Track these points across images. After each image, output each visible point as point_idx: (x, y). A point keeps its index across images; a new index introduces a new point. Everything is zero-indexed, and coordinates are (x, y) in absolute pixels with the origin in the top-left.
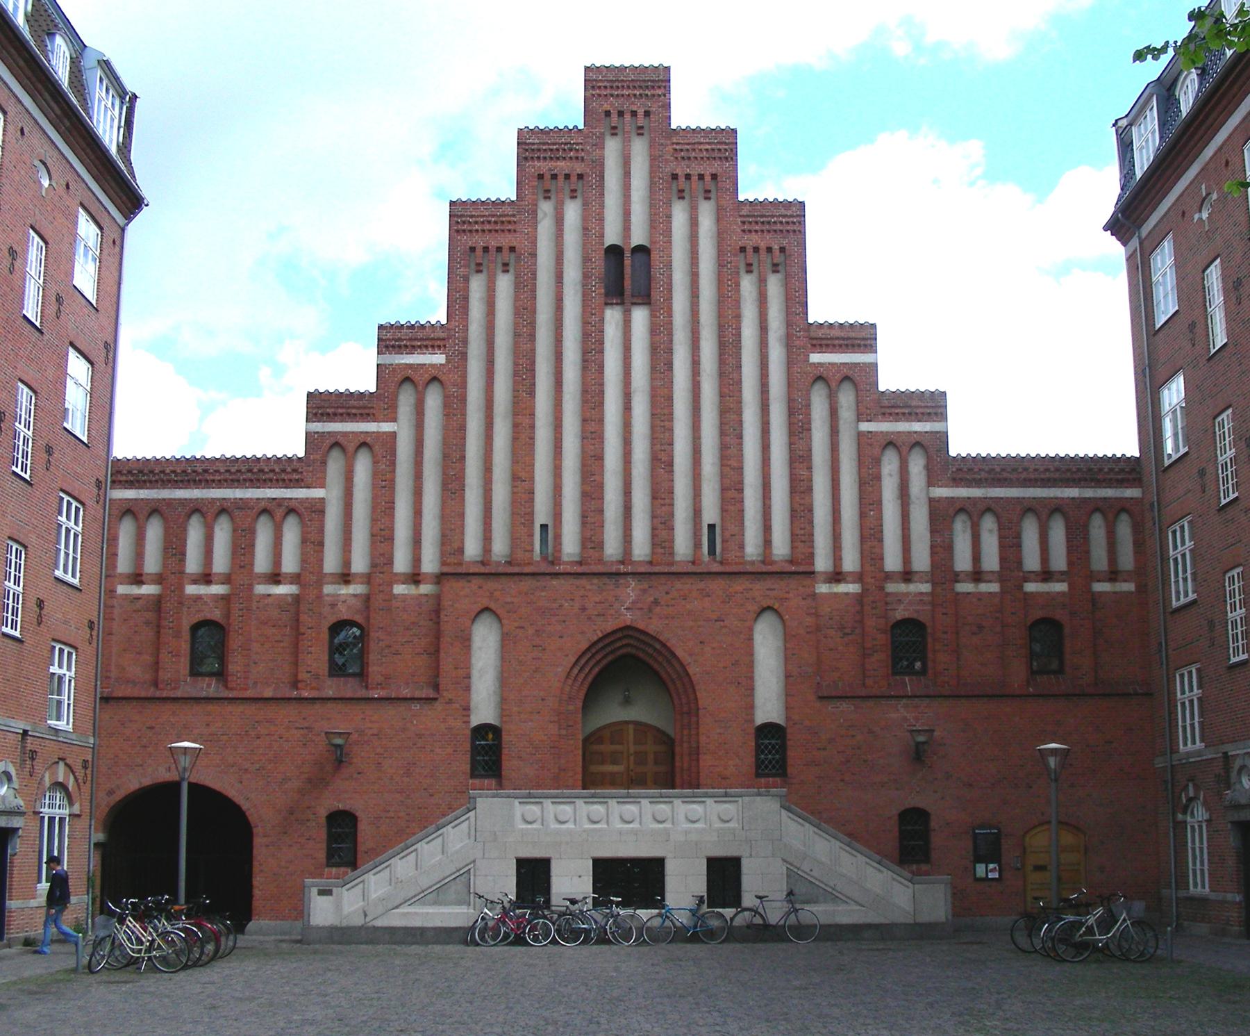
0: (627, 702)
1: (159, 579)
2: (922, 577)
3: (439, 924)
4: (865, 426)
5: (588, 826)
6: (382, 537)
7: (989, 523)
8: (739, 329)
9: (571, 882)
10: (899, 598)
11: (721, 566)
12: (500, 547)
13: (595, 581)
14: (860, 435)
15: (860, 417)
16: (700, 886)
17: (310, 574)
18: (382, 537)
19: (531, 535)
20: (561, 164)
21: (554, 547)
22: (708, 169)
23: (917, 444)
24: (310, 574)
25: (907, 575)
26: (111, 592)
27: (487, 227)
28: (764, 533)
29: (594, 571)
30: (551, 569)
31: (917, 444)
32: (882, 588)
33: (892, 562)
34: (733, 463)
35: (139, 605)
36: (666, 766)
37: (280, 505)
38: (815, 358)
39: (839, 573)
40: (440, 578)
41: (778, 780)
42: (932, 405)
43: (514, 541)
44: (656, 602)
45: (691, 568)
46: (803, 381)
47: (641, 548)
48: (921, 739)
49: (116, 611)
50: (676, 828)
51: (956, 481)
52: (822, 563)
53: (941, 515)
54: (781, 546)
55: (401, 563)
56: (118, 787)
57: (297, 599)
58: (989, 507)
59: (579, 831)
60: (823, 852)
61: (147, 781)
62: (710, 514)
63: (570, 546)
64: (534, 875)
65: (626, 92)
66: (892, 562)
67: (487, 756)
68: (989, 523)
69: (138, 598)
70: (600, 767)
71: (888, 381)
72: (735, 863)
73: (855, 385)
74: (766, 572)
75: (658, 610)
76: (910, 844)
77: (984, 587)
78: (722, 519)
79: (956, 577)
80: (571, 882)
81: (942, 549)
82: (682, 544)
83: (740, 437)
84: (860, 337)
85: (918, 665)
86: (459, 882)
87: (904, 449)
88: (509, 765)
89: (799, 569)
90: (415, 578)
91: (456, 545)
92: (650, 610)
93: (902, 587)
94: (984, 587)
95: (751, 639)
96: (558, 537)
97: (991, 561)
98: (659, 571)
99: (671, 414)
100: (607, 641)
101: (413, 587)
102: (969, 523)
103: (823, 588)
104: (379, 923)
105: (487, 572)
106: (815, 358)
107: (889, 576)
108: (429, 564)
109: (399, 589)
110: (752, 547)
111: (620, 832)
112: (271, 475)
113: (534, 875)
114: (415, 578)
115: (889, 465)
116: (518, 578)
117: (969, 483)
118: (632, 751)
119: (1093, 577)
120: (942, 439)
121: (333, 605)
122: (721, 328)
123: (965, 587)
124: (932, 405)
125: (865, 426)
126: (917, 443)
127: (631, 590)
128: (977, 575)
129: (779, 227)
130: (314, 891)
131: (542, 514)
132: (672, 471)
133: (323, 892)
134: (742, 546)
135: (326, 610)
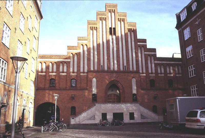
0: (112, 91)
1: (45, 72)
2: (65, 72)
3: (90, 123)
4: (145, 53)
5: (112, 108)
6: (79, 67)
7: (65, 65)
8: (128, 39)
9: (110, 117)
10: (151, 76)
11: (127, 71)
12: (96, 68)
13: (109, 73)
14: (145, 54)
15: (145, 52)
16: (101, 117)
17: (68, 72)
18: (79, 67)
19: (100, 67)
20: (103, 16)
21: (103, 69)
22: (123, 18)
23: (152, 55)
24: (68, 72)
25: (152, 73)
26: (38, 74)
27: (93, 24)
28: (133, 67)
29: (109, 72)
30: (103, 71)
31: (152, 55)
32: (149, 75)
33: (71, 70)
34: (118, 56)
35: (42, 76)
36: (119, 100)
37: (63, 62)
38: (138, 43)
39: (64, 72)
40: (87, 73)
41: (136, 102)
42: (154, 50)
43: (123, 68)
44: (118, 76)
45: (122, 72)
46: (137, 47)
47: (116, 69)
48: (156, 96)
49: (39, 77)
50: (125, 108)
51: (158, 61)
52: (141, 71)
53: (156, 65)
54: (135, 69)
55: (82, 70)
56: (39, 103)
57: (45, 75)
58: (162, 64)
59: (110, 109)
60: (146, 112)
61: (43, 102)
62: (125, 64)
63: (106, 68)
64: (104, 116)
65: (111, 7)
66: (150, 71)
67: (95, 99)
68: (65, 65)
69: (42, 75)
70: (107, 100)
71: (148, 47)
72: (133, 113)
73: (144, 47)
74: (133, 72)
75: (118, 77)
76: (154, 110)
77: (162, 75)
78: (127, 65)
79: (159, 73)
80: (110, 117)
81: (156, 70)
82: (122, 69)
83: (129, 54)
84: (144, 41)
85: (171, 86)
86: (93, 118)
87: (151, 56)
88: (98, 99)
89: (137, 72)
90: (84, 72)
91: (90, 68)
92: (117, 78)
93: (151, 75)
94: (162, 75)
95: (131, 82)
96: (104, 67)
97: (163, 71)
98: (119, 72)
99: (119, 50)
100: (112, 82)
101: (83, 74)
102: (159, 66)
103: (160, 75)
104: (81, 123)
105: (93, 72)
106: (138, 43)
107: (150, 73)
108: (86, 71)
109: (82, 74)
110: (131, 69)
111: (117, 109)
112: (62, 57)
113: (104, 116)
114: (84, 72)
115: (149, 58)
116: (100, 72)
117: (159, 61)
118: (113, 98)
119: (81, 73)
120: (156, 55)
121: (72, 76)
122: (125, 39)
123: (160, 75)
124: (154, 50)
125: (145, 53)
126: (152, 55)
127: (115, 75)
128: (161, 73)
129: (133, 26)
130: (71, 118)
131: (102, 64)
132: (120, 58)
133: (72, 119)
134: (130, 69)
135: (71, 77)
